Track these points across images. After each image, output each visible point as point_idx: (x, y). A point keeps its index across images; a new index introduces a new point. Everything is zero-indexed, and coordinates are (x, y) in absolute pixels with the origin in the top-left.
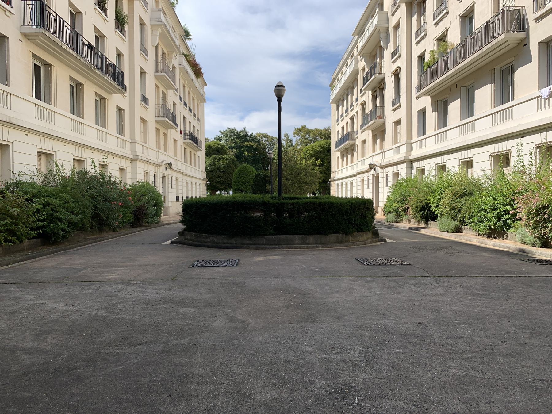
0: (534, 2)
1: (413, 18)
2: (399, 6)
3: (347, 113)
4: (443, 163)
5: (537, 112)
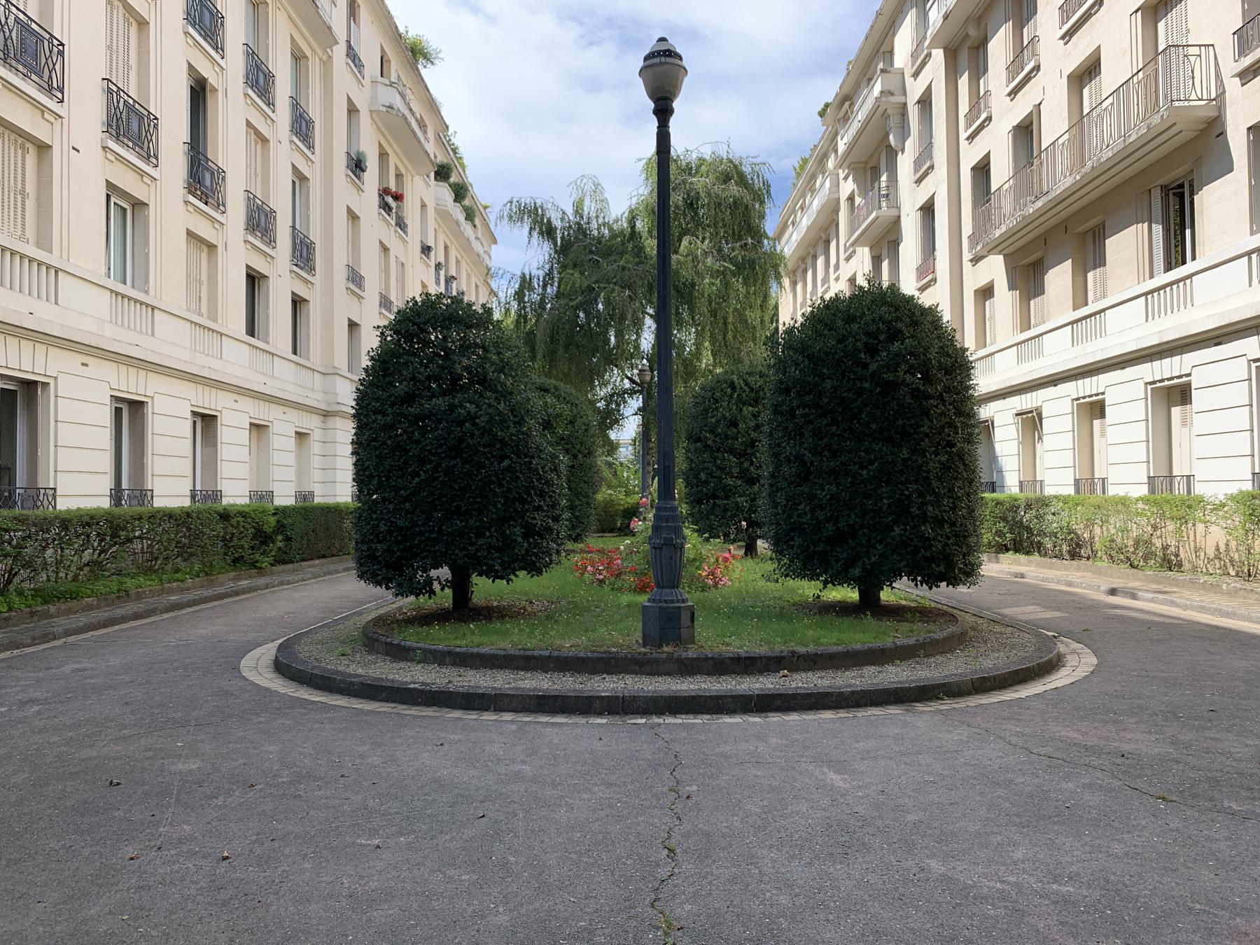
0: (1236, 36)
1: (959, 82)
2: (929, 55)
3: (826, 286)
4: (1097, 395)
5: (1250, 286)
